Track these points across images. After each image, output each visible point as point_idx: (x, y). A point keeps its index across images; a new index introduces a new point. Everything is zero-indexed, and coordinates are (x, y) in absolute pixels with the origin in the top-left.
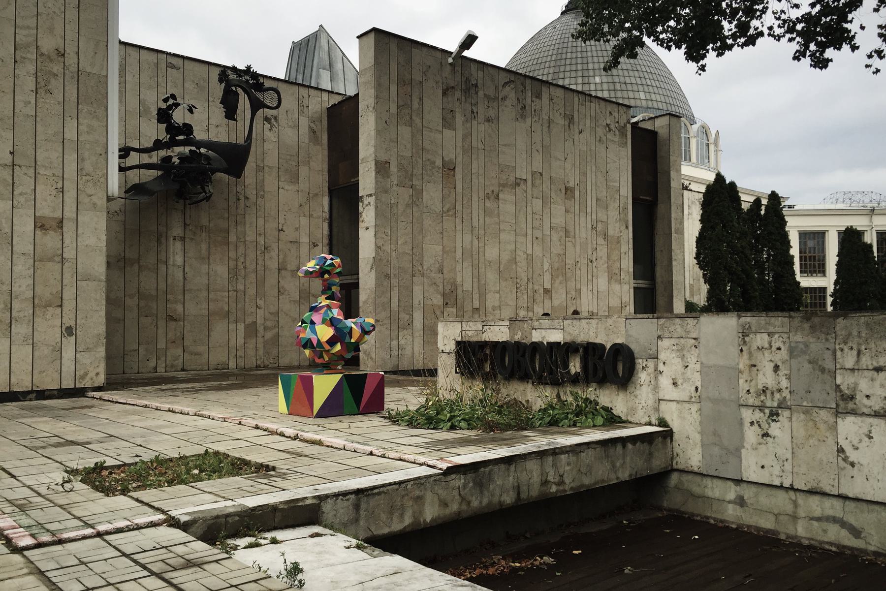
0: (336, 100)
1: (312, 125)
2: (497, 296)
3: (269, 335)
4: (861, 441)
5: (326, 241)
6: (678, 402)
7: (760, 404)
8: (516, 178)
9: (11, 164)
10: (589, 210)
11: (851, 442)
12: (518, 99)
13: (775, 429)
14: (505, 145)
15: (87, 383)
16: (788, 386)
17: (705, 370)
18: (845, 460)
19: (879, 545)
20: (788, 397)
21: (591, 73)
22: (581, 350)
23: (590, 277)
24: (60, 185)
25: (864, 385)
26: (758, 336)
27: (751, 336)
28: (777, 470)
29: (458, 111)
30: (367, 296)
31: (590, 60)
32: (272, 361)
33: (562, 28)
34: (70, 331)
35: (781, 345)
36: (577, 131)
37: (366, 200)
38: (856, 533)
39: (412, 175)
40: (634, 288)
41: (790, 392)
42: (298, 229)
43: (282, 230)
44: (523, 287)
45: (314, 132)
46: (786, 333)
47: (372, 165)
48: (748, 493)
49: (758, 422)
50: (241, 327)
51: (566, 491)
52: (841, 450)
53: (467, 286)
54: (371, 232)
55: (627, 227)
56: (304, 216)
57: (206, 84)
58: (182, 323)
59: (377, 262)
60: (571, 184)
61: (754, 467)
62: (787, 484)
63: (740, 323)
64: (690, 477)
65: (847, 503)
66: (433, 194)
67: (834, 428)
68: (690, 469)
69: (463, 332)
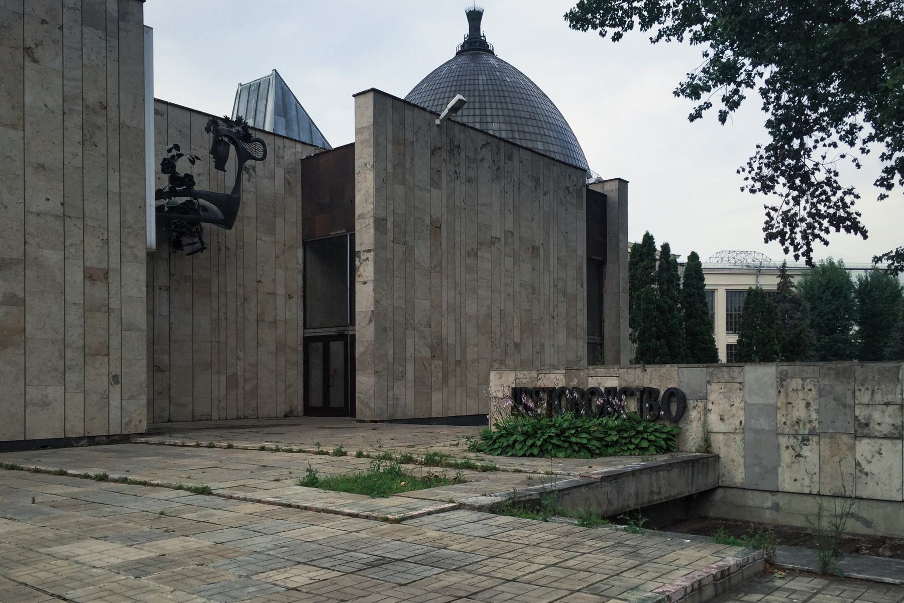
0: (311, 152)
1: (287, 176)
2: (476, 349)
3: (248, 387)
4: (873, 457)
5: (301, 293)
6: (724, 433)
7: (794, 432)
8: (492, 237)
9: (62, 215)
10: (551, 268)
11: (865, 458)
12: (494, 160)
13: (806, 451)
14: (483, 205)
15: (131, 430)
16: (818, 418)
17: (748, 407)
18: (861, 471)
19: (885, 532)
20: (817, 426)
21: (489, 119)
22: (638, 394)
23: (552, 332)
24: (105, 237)
25: (877, 416)
26: (794, 380)
27: (787, 380)
28: (807, 482)
29: (444, 170)
30: (364, 348)
31: (488, 105)
32: (251, 413)
33: (459, 70)
34: (116, 379)
35: (812, 387)
36: (542, 192)
37: (364, 256)
38: (867, 523)
39: (405, 233)
40: (588, 343)
41: (819, 423)
42: (274, 281)
43: (260, 281)
44: (497, 342)
45: (289, 183)
46: (816, 378)
47: (371, 221)
48: (782, 500)
49: (792, 446)
50: (223, 378)
51: (661, 499)
52: (858, 464)
53: (451, 341)
54: (370, 287)
55: (582, 286)
56: (281, 267)
57: (188, 131)
58: (168, 374)
59: (376, 315)
60: (537, 244)
61: (788, 480)
62: (815, 491)
63: (779, 370)
64: (734, 491)
65: (862, 502)
66: (422, 251)
67: (853, 448)
68: (735, 485)
69: (517, 380)
